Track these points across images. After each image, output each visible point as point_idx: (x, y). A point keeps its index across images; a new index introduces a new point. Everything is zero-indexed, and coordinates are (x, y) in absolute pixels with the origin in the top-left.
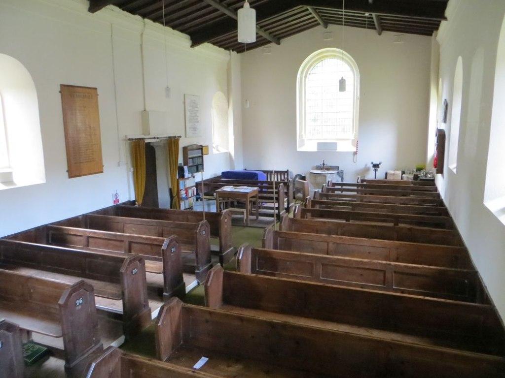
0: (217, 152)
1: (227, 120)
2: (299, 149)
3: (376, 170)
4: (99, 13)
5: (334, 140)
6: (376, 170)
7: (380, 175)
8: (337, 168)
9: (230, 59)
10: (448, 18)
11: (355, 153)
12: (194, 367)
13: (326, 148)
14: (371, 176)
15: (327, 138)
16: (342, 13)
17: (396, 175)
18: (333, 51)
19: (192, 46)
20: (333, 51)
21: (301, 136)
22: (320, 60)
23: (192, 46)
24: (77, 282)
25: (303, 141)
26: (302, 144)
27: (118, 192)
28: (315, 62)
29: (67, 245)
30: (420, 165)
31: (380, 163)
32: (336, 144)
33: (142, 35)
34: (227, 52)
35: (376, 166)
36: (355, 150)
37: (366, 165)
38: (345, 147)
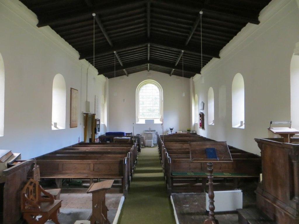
0: (55, 129)
1: (104, 109)
2: (136, 123)
3: (171, 131)
4: (81, 60)
5: (152, 119)
6: (171, 131)
7: (174, 132)
8: (155, 131)
9: (106, 81)
10: (202, 74)
11: (162, 124)
12: (260, 155)
13: (149, 122)
14: (170, 133)
15: (150, 118)
16: (113, 60)
17: (178, 132)
18: (151, 81)
19: (98, 75)
20: (151, 81)
21: (137, 117)
22: (145, 84)
23: (98, 75)
24: (4, 209)
25: (138, 119)
26: (138, 121)
27: (173, 129)
28: (143, 84)
29: (64, 172)
30: (188, 129)
31: (173, 128)
32: (154, 120)
33: (88, 69)
34: (105, 78)
35: (171, 129)
36: (162, 123)
37: (167, 129)
38: (158, 121)
